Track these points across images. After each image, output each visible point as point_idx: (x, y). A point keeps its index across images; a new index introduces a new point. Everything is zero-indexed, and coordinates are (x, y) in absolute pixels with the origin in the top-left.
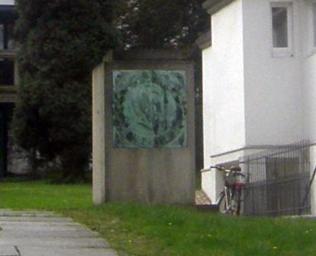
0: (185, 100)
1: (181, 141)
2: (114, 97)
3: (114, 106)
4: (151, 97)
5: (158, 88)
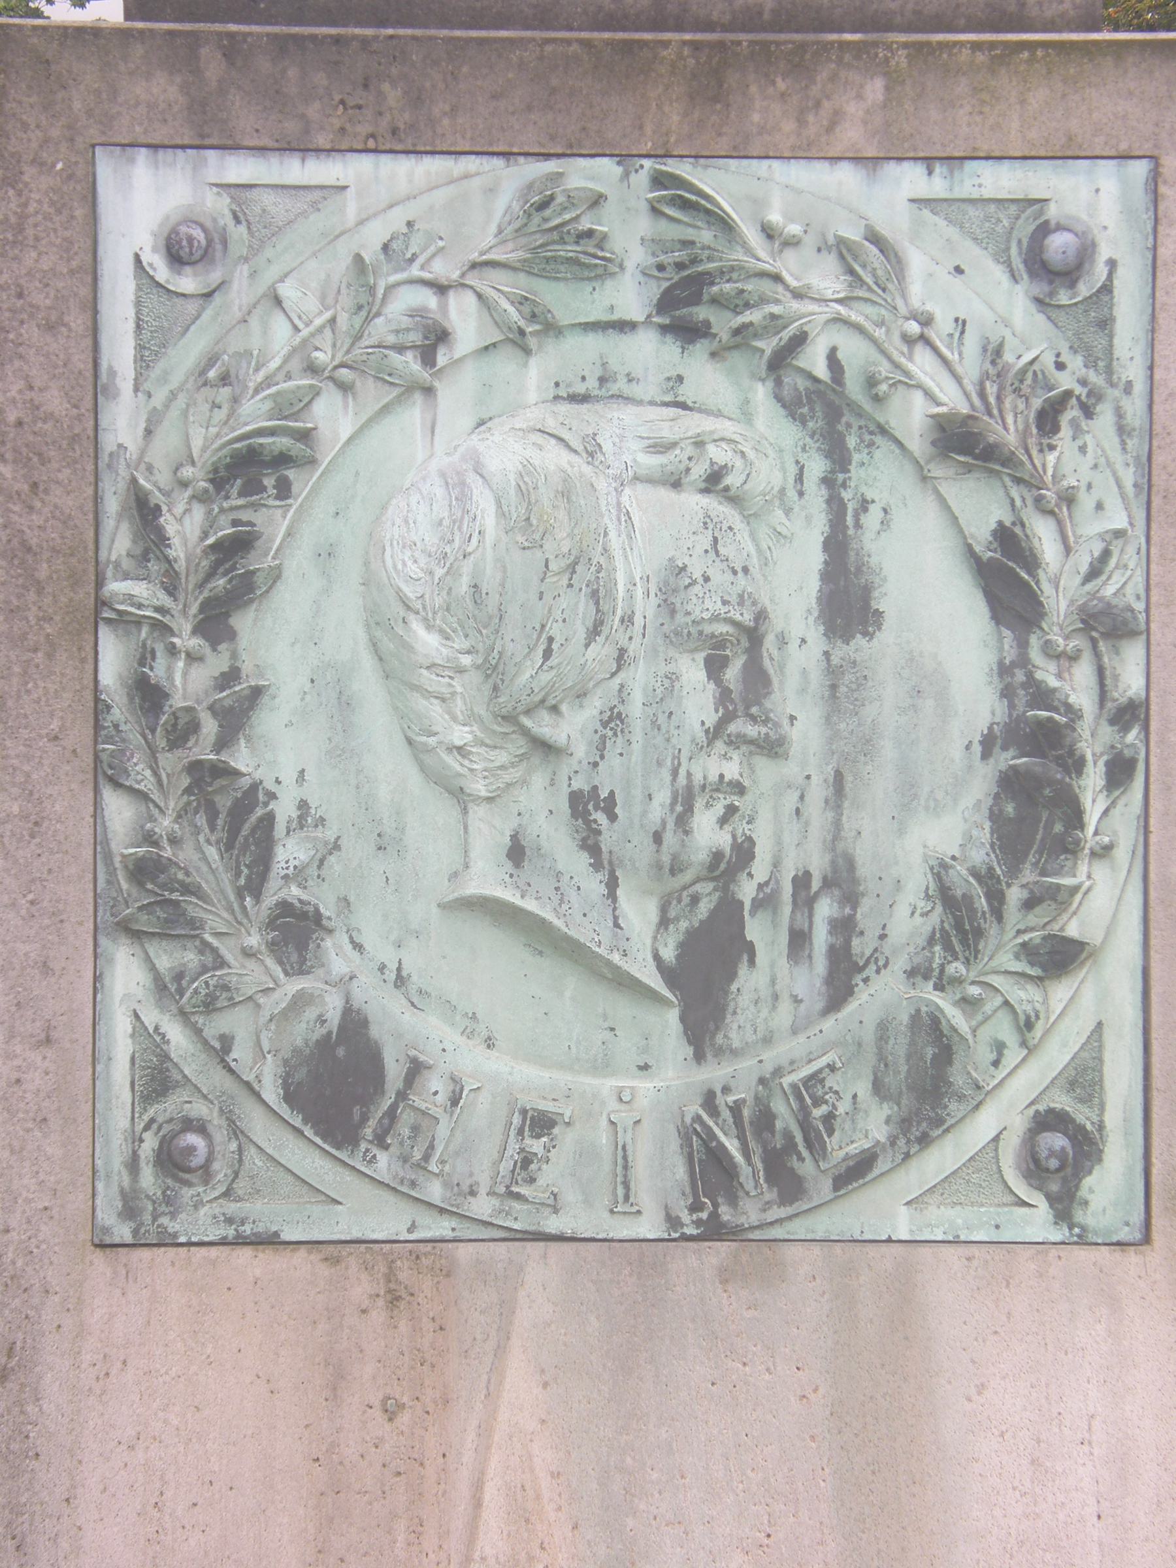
0: (1122, 585)
1: (1059, 1154)
2: (120, 542)
3: (113, 660)
4: (648, 535)
5: (762, 439)
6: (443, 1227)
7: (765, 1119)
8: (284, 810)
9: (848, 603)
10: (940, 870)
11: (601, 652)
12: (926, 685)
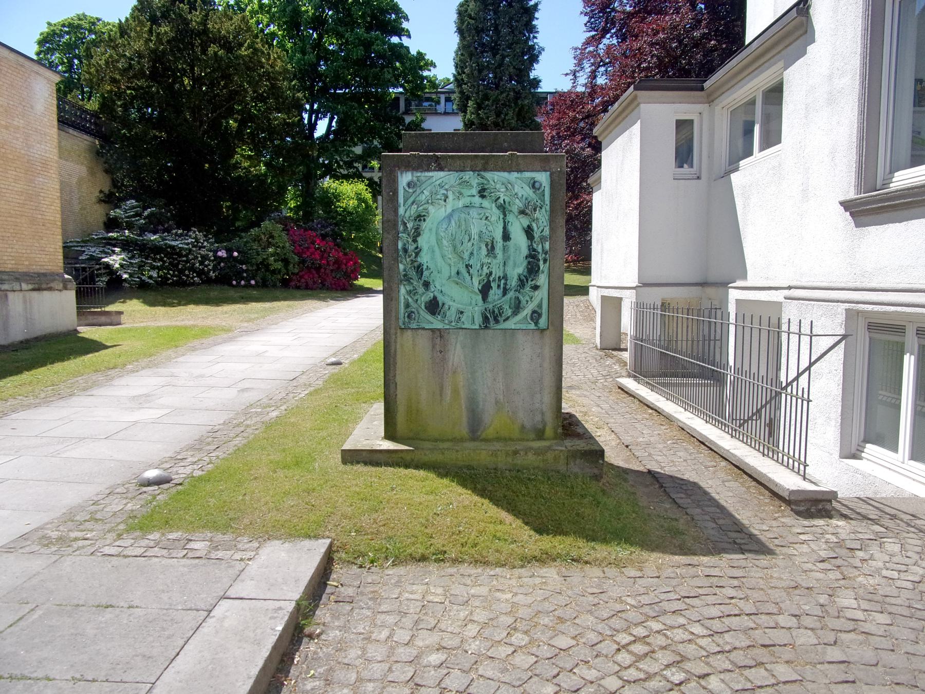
2: (401, 228)
6: (448, 327)
7: (494, 312)
8: (425, 267)
9: (506, 237)
10: (519, 276)
11: (470, 244)
12: (518, 249)
